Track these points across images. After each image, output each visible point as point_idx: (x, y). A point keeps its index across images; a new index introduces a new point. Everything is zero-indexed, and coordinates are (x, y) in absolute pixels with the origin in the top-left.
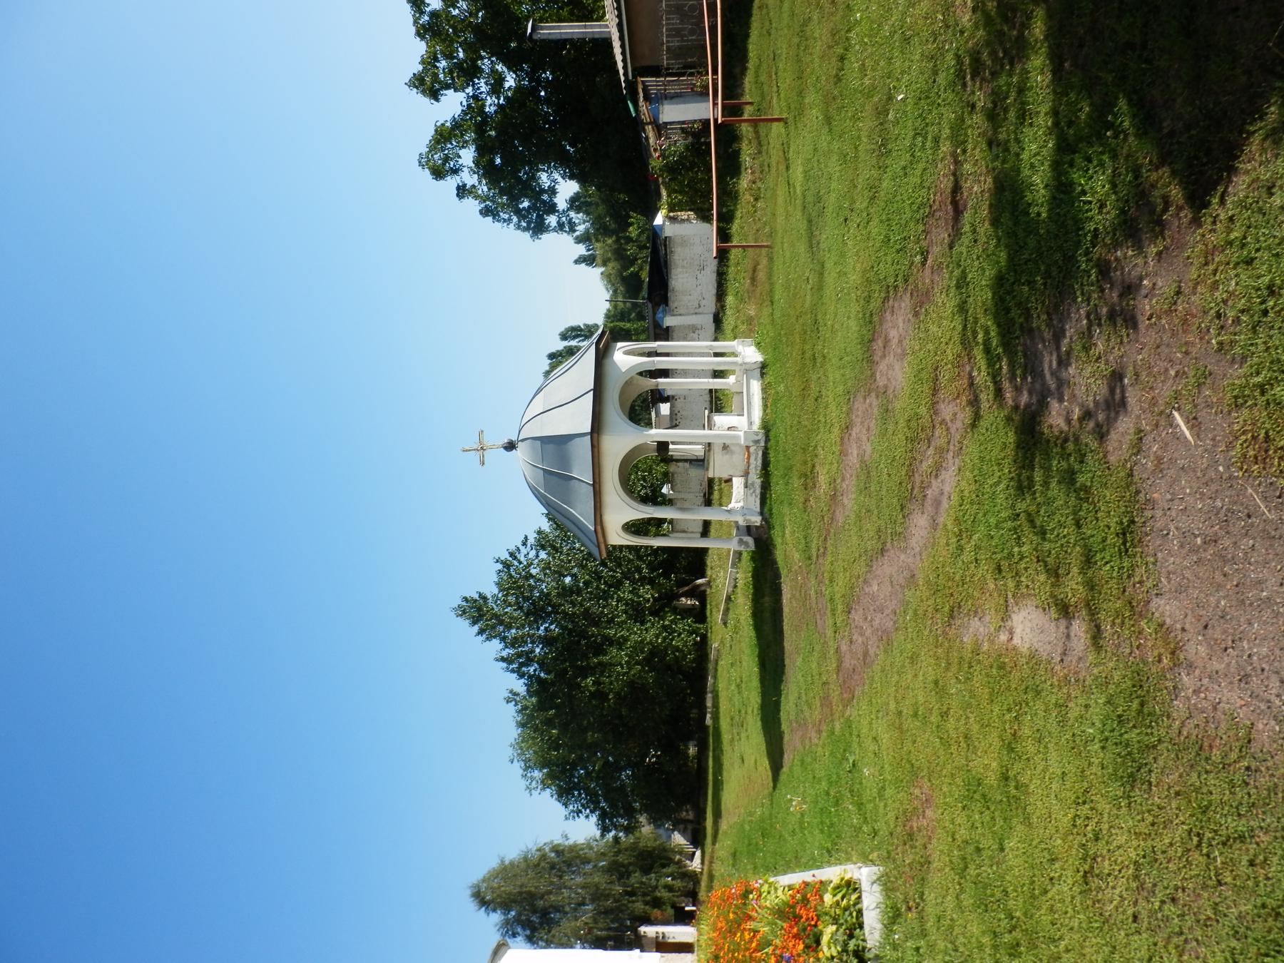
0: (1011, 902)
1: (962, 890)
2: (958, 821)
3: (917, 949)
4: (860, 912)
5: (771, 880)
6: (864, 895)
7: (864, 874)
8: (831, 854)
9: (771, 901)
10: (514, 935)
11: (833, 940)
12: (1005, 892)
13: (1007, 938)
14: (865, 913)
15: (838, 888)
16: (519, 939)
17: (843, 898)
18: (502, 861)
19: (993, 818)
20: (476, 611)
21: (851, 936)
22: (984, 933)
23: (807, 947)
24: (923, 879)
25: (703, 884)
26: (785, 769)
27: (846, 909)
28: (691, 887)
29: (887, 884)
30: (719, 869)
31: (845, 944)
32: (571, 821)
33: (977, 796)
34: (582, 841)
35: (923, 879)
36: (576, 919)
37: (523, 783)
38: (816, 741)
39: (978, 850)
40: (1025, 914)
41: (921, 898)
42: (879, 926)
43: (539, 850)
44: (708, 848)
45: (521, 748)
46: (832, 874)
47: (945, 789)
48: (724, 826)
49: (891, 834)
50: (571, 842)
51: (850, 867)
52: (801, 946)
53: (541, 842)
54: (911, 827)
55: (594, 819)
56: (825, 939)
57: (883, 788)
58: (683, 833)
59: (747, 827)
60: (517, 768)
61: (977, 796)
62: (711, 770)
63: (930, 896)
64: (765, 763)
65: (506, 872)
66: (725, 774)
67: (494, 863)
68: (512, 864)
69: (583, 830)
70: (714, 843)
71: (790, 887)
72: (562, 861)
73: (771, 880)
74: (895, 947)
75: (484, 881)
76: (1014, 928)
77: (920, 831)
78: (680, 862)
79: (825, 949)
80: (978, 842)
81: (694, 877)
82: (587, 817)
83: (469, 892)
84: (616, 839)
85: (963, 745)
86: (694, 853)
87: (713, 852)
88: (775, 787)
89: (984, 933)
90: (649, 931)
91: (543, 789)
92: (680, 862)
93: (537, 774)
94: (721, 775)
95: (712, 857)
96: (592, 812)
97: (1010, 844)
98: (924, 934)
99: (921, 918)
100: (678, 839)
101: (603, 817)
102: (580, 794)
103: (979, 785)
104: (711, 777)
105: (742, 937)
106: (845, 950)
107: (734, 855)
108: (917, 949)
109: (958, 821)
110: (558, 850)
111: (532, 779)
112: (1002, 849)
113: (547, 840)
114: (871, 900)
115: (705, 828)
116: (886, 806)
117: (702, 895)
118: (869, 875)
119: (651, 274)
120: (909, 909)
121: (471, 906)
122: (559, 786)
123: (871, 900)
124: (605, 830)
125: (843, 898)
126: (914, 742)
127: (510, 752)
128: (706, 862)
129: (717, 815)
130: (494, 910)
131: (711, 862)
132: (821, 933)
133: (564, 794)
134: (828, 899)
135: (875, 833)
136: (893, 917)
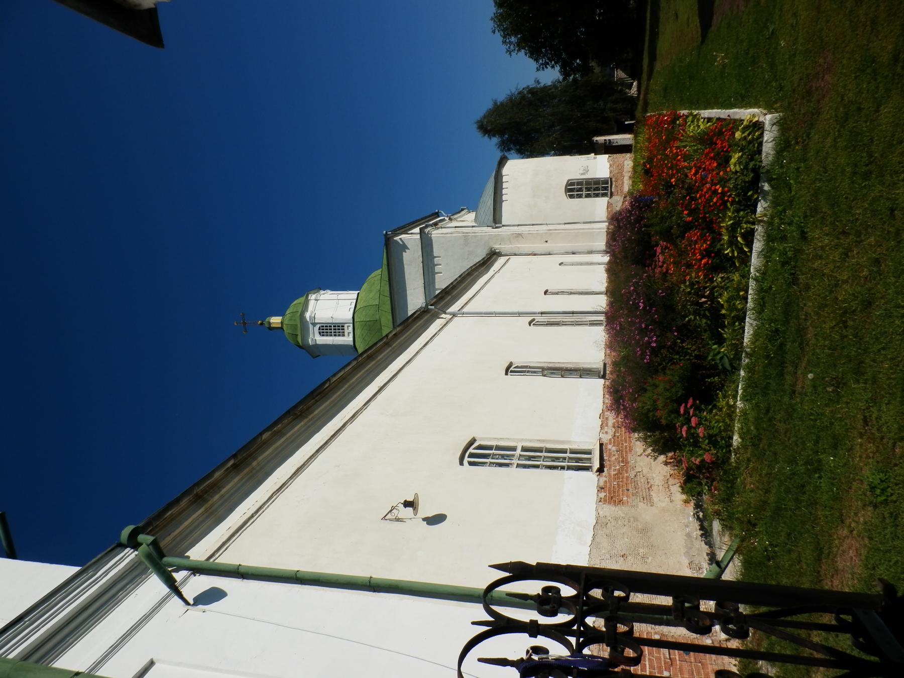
0: (873, 147)
1: (840, 136)
2: (850, 87)
3: (798, 169)
4: (761, 144)
5: (695, 112)
6: (766, 133)
7: (768, 119)
8: (744, 101)
9: (691, 130)
10: (509, 150)
11: (739, 161)
12: (872, 140)
13: (864, 169)
14: (764, 144)
15: (746, 128)
16: (512, 152)
17: (749, 135)
18: (495, 103)
19: (877, 88)
20: (538, 70)
21: (752, 159)
22: (848, 164)
23: (719, 165)
24: (812, 124)
25: (639, 108)
26: (713, 28)
27: (750, 142)
28: (630, 107)
29: (782, 125)
30: (652, 97)
31: (747, 164)
32: (541, 72)
33: (869, 71)
34: (550, 83)
35: (812, 124)
36: (549, 136)
37: (504, 48)
38: (743, 8)
39: (859, 109)
40: (882, 156)
41: (808, 136)
42: (772, 152)
43: (520, 93)
44: (644, 83)
45: (500, 21)
46: (745, 114)
47: (845, 62)
48: (658, 66)
49: (794, 91)
50: (542, 85)
51: (756, 110)
52: (715, 165)
53: (521, 87)
54: (811, 86)
55: (558, 68)
56: (733, 161)
57: (794, 55)
58: (624, 70)
59: (677, 70)
60: (498, 36)
61: (869, 71)
62: (648, 21)
63: (816, 137)
64: (696, 21)
65: (499, 110)
66: (661, 26)
67: (489, 105)
68: (502, 104)
69: (551, 75)
70: (649, 79)
71: (709, 120)
72: (534, 98)
73: (695, 112)
74: (782, 167)
75: (485, 117)
76: (871, 163)
77: (817, 89)
78: (621, 90)
79: (732, 167)
80: (860, 103)
81: (633, 101)
82: (553, 67)
83: (475, 126)
84: (575, 80)
85: (869, 28)
86: (632, 84)
87: (648, 85)
88: (703, 41)
89: (848, 164)
90: (600, 139)
91: (519, 50)
92: (621, 90)
93: (513, 39)
94: (658, 28)
95: (647, 89)
96: (556, 63)
97: (884, 110)
98: (805, 160)
99: (805, 149)
100: (619, 74)
101: (563, 67)
102: (546, 51)
103: (873, 62)
104: (648, 27)
105: (671, 151)
106: (746, 167)
107: (665, 89)
108: (798, 169)
109: (850, 87)
110: (532, 91)
111: (510, 43)
112: (877, 111)
113: (525, 86)
114: (769, 137)
115: (642, 66)
116: (793, 69)
117: (638, 114)
118: (771, 120)
119: (818, 652)
120: (797, 143)
121: (478, 135)
122: (529, 47)
123: (769, 137)
124: (566, 74)
125: (749, 135)
126: (828, 21)
127: (491, 24)
128: (642, 92)
129: (653, 58)
130: (494, 136)
131: (646, 94)
132: (730, 157)
133: (535, 54)
134: (738, 135)
135: (781, 88)
136: (783, 146)
